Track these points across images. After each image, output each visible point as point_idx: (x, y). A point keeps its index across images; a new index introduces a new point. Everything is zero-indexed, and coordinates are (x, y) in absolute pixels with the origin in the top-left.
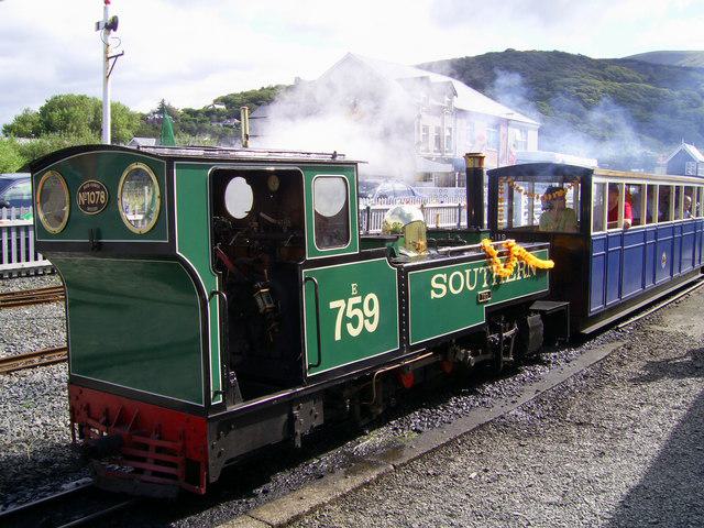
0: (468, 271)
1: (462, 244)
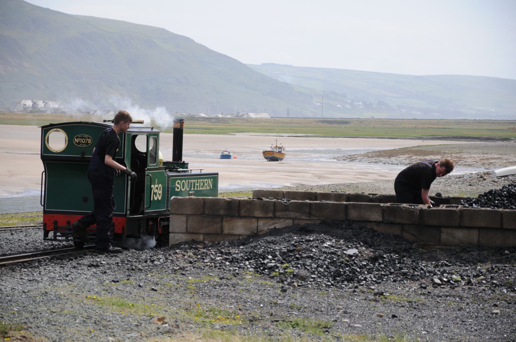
0: (187, 181)
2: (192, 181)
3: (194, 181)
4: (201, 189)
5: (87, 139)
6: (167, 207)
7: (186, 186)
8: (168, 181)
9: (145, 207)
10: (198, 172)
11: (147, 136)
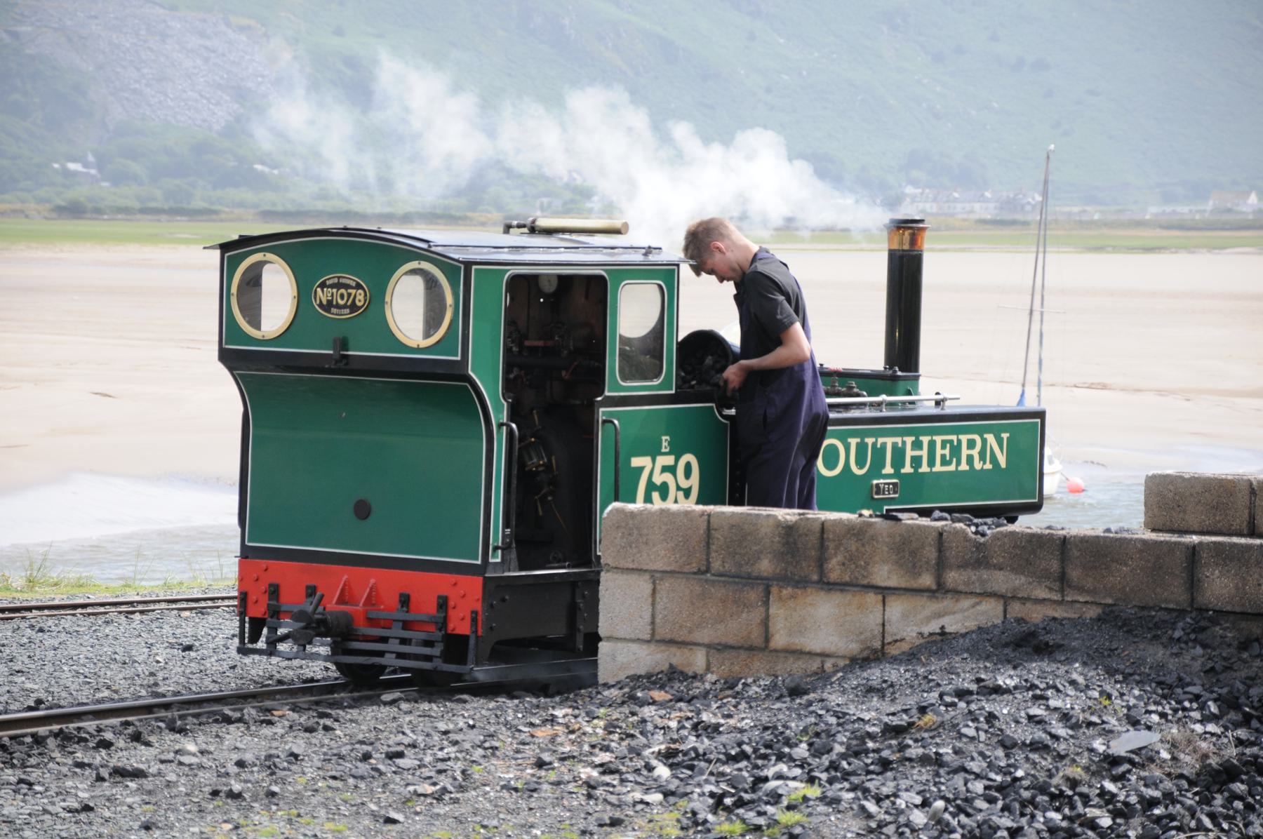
0: (853, 442)
1: (858, 395)
4: (938, 468)
5: (353, 292)
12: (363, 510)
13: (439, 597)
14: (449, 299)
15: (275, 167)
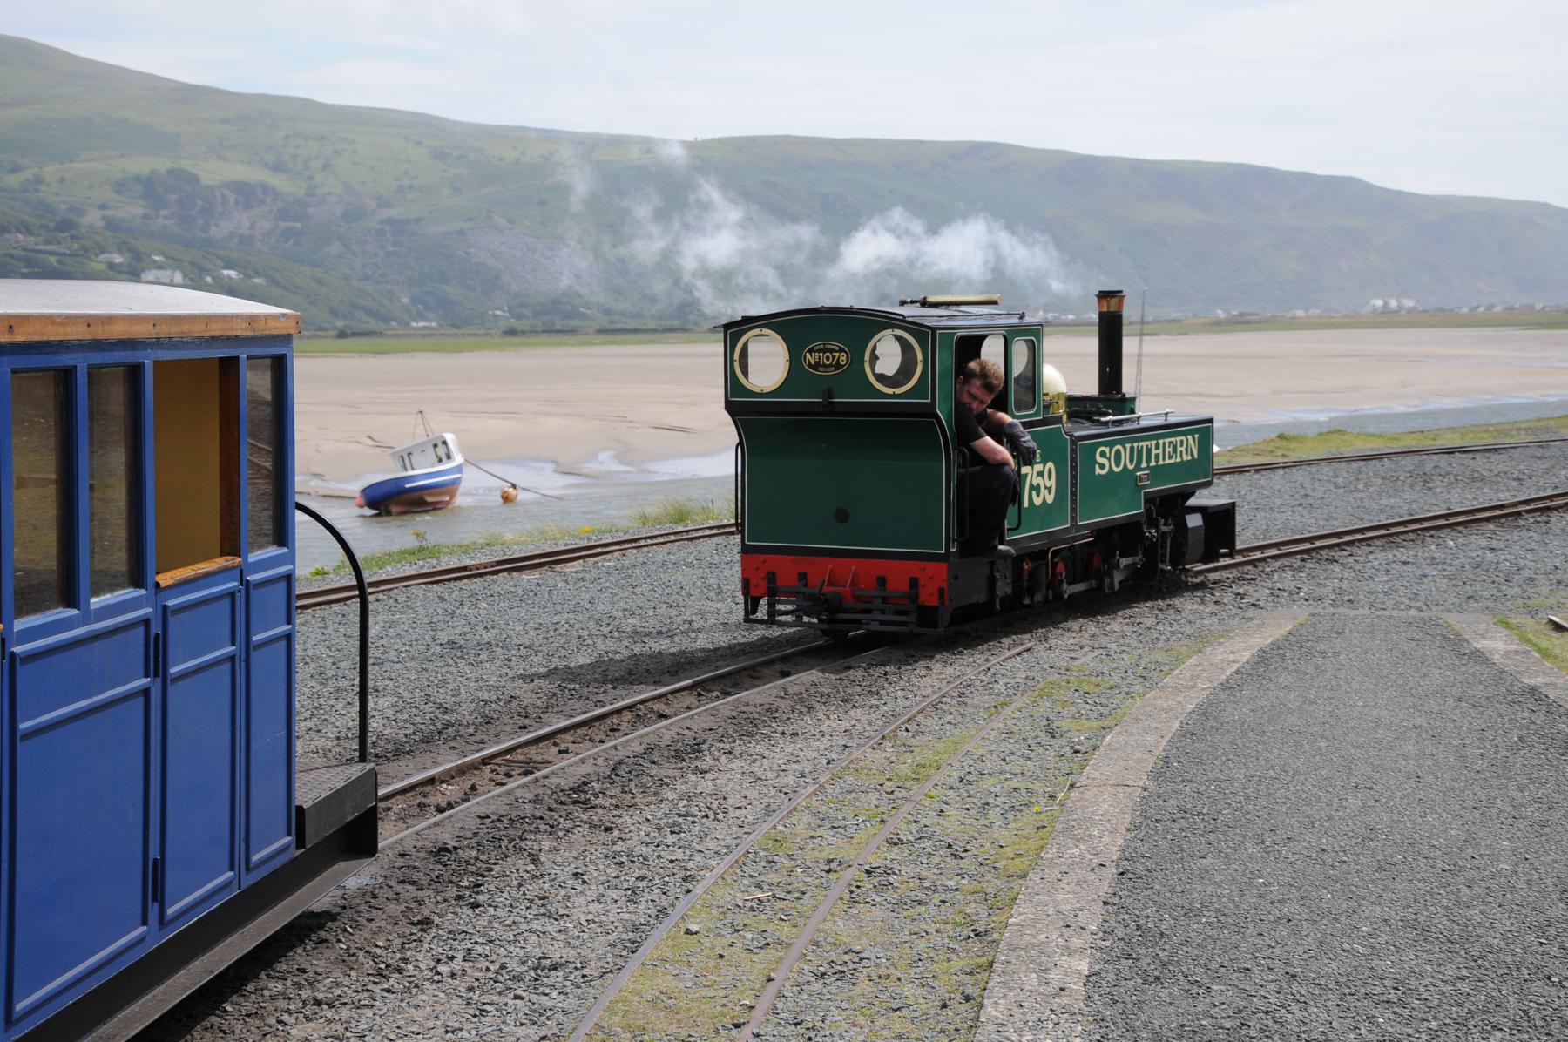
0: (1128, 446)
2: (1141, 444)
3: (1148, 443)
4: (1168, 461)
5: (837, 354)
6: (1074, 519)
7: (1125, 457)
8: (1073, 451)
9: (1006, 527)
10: (1160, 421)
11: (1004, 336)
12: (842, 516)
13: (911, 579)
14: (920, 357)
15: (589, 309)
